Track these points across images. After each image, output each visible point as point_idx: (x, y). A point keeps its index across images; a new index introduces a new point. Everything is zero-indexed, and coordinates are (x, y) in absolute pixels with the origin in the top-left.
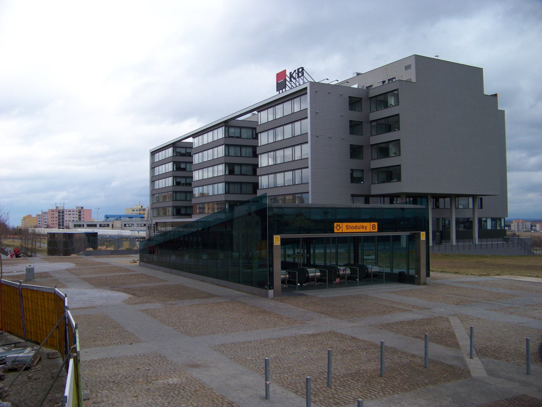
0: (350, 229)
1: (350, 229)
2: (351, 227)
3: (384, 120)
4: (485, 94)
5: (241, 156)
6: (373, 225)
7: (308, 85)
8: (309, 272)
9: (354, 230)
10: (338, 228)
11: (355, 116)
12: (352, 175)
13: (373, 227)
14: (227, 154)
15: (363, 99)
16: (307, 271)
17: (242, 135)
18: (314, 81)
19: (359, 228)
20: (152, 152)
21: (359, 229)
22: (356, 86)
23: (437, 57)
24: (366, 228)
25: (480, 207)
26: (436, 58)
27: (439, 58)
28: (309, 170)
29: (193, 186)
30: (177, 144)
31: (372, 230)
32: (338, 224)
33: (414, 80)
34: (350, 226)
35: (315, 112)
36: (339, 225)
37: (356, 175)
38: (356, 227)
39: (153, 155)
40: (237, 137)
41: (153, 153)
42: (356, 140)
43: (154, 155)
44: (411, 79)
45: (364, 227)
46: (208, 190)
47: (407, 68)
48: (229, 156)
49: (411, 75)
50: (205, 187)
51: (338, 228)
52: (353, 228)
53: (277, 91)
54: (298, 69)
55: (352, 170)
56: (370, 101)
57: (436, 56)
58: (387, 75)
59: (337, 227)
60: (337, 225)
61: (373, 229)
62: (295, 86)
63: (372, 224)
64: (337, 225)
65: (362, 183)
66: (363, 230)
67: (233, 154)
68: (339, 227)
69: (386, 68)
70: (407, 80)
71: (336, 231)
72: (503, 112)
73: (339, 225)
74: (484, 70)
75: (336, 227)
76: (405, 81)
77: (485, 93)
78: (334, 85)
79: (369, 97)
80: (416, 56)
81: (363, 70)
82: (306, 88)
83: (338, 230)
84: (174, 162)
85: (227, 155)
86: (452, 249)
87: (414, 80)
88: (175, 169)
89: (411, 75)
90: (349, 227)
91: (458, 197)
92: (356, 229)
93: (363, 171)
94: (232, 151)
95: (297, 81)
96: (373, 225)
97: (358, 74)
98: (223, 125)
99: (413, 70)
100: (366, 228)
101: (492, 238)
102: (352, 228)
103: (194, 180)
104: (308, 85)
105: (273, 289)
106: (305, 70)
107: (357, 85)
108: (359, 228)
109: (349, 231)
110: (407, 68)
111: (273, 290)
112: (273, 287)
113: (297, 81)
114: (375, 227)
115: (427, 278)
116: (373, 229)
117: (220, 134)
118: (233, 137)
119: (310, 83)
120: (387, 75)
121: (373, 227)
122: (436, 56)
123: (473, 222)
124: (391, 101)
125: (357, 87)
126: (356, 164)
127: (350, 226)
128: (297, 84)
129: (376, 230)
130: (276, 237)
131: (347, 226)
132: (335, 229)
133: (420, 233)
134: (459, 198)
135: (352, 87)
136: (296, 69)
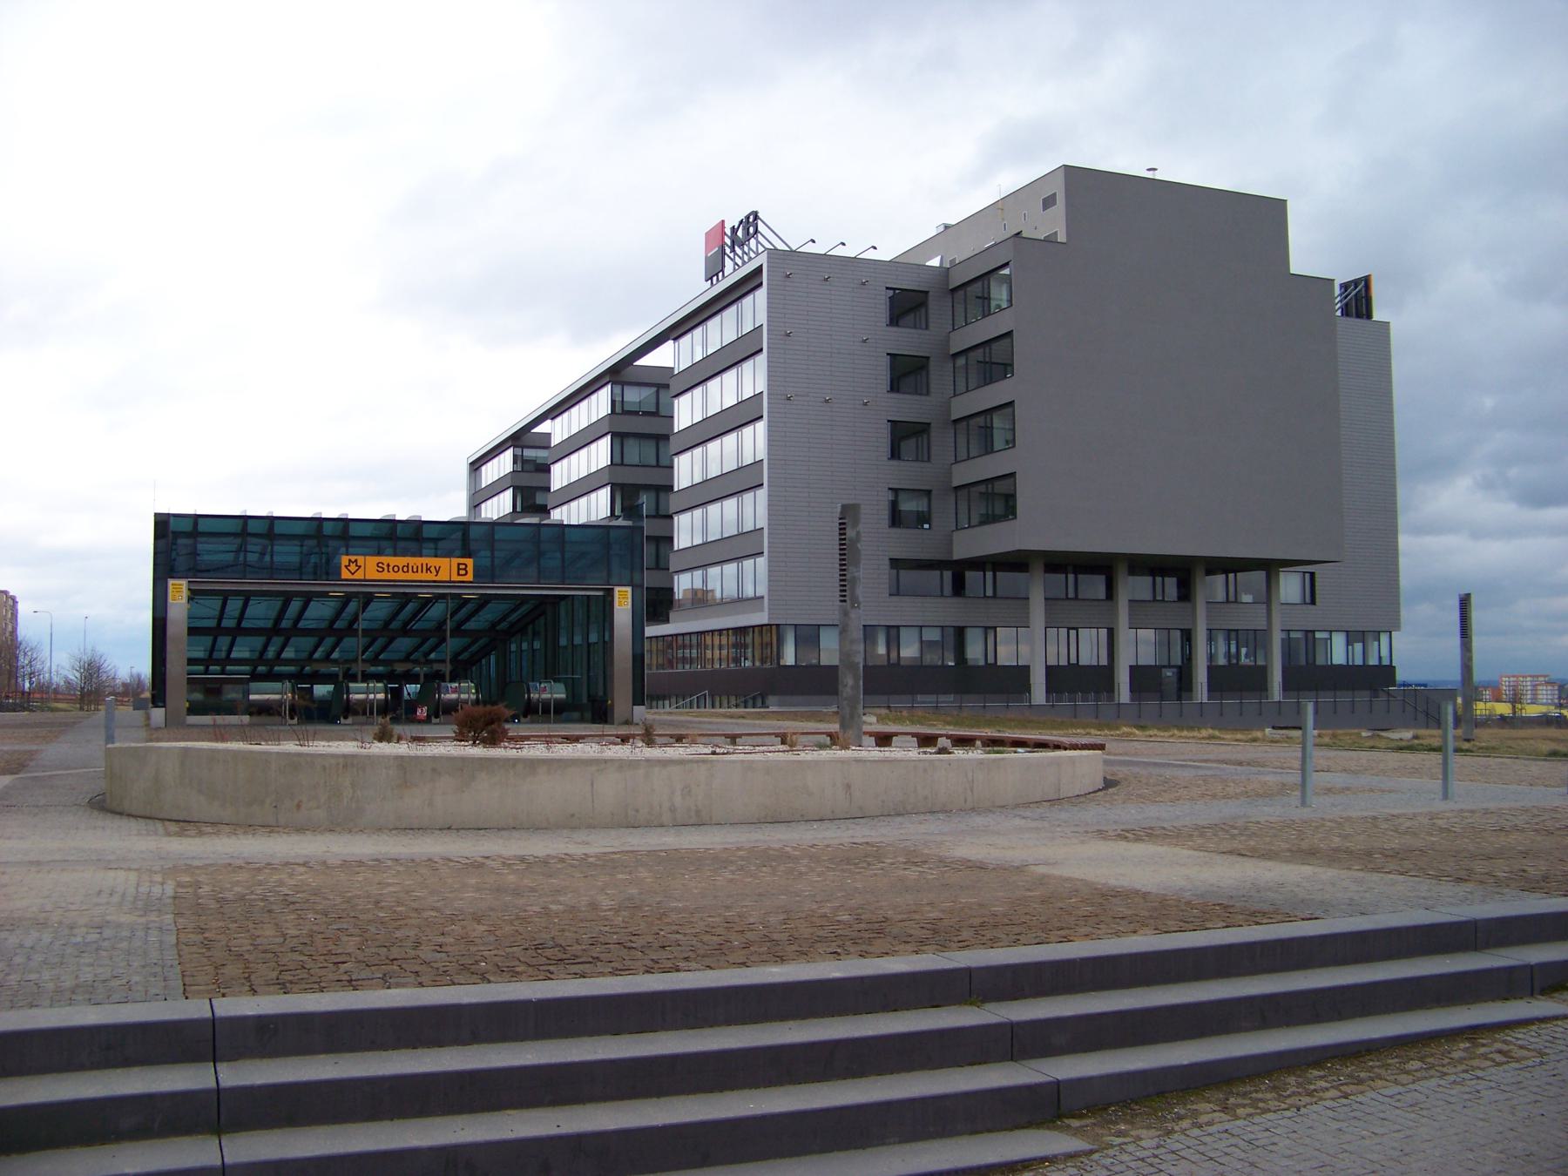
0: (389, 571)
1: (389, 571)
2: (391, 568)
3: (981, 351)
4: (1292, 272)
5: (658, 466)
6: (459, 564)
7: (762, 260)
8: (351, 690)
9: (401, 576)
10: (353, 567)
11: (907, 340)
12: (894, 505)
13: (459, 569)
14: (617, 460)
15: (931, 294)
16: (348, 687)
17: (660, 409)
18: (772, 248)
19: (415, 570)
20: (472, 464)
21: (417, 571)
22: (935, 262)
23: (1151, 172)
24: (437, 572)
25: (1308, 599)
26: (1149, 175)
27: (1159, 176)
28: (762, 494)
29: (671, 570)
30: (525, 436)
31: (455, 578)
32: (353, 558)
33: (1062, 238)
34: (388, 565)
35: (783, 333)
36: (356, 561)
37: (907, 505)
38: (408, 567)
39: (477, 469)
40: (646, 414)
41: (476, 465)
42: (908, 407)
43: (478, 472)
44: (1056, 233)
45: (433, 569)
46: (722, 580)
47: (1049, 202)
48: (622, 464)
49: (1054, 224)
50: (714, 571)
51: (353, 567)
52: (396, 569)
53: (707, 281)
54: (748, 217)
55: (895, 491)
56: (953, 298)
57: (1149, 170)
58: (1005, 225)
59: (349, 565)
60: (350, 561)
61: (459, 574)
62: (740, 264)
63: (455, 561)
64: (350, 561)
65: (926, 526)
66: (430, 577)
67: (636, 461)
68: (356, 565)
69: (1000, 207)
70: (1048, 236)
71: (345, 574)
72: (1386, 325)
73: (356, 561)
74: (1289, 205)
75: (346, 566)
76: (1044, 241)
77: (1295, 268)
78: (890, 261)
79: (950, 288)
80: (1069, 170)
81: (953, 220)
82: (759, 270)
83: (353, 574)
84: (516, 489)
85: (618, 461)
86: (1181, 712)
87: (1062, 238)
88: (519, 509)
89: (1054, 224)
90: (386, 568)
91: (1235, 572)
92: (408, 571)
93: (928, 493)
94: (633, 451)
95: (753, 251)
96: (459, 564)
97: (947, 227)
98: (608, 380)
99: (1060, 206)
100: (437, 572)
101: (1353, 689)
102: (396, 569)
103: (676, 548)
104: (762, 260)
105: (164, 706)
106: (762, 218)
107: (939, 258)
108: (415, 570)
109: (385, 576)
110: (1049, 202)
111: (164, 709)
112: (164, 702)
113: (753, 251)
114: (465, 569)
115: (635, 707)
116: (459, 574)
117: (599, 405)
118: (636, 413)
119: (768, 253)
120: (1005, 225)
121: (461, 569)
122: (1149, 170)
123: (1193, 632)
124: (999, 294)
125: (938, 265)
126: (906, 473)
127: (388, 565)
128: (746, 258)
129: (470, 577)
130: (175, 585)
131: (380, 565)
132: (344, 571)
133: (613, 589)
134: (1238, 574)
135: (927, 264)
136: (742, 217)
